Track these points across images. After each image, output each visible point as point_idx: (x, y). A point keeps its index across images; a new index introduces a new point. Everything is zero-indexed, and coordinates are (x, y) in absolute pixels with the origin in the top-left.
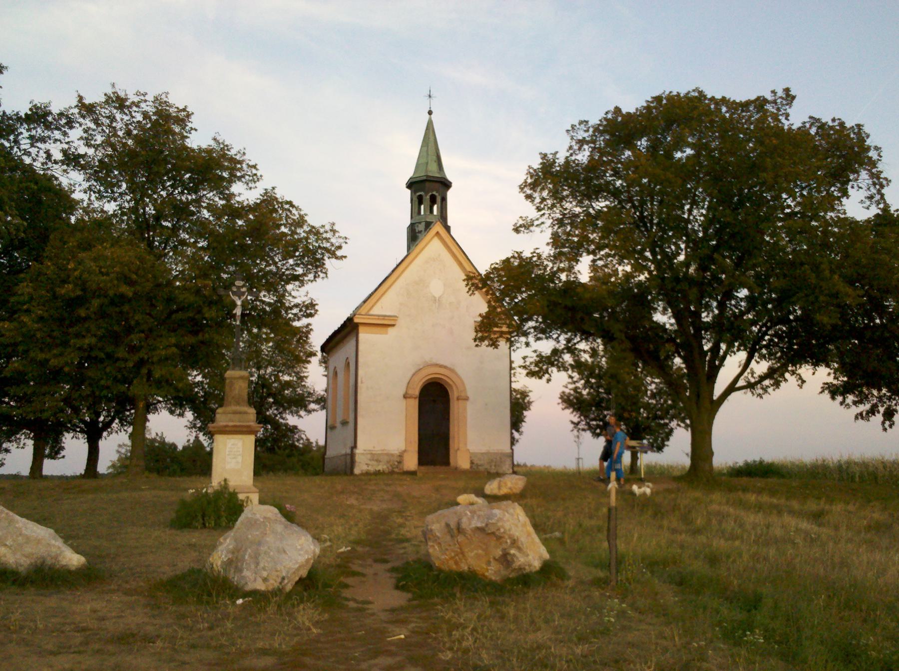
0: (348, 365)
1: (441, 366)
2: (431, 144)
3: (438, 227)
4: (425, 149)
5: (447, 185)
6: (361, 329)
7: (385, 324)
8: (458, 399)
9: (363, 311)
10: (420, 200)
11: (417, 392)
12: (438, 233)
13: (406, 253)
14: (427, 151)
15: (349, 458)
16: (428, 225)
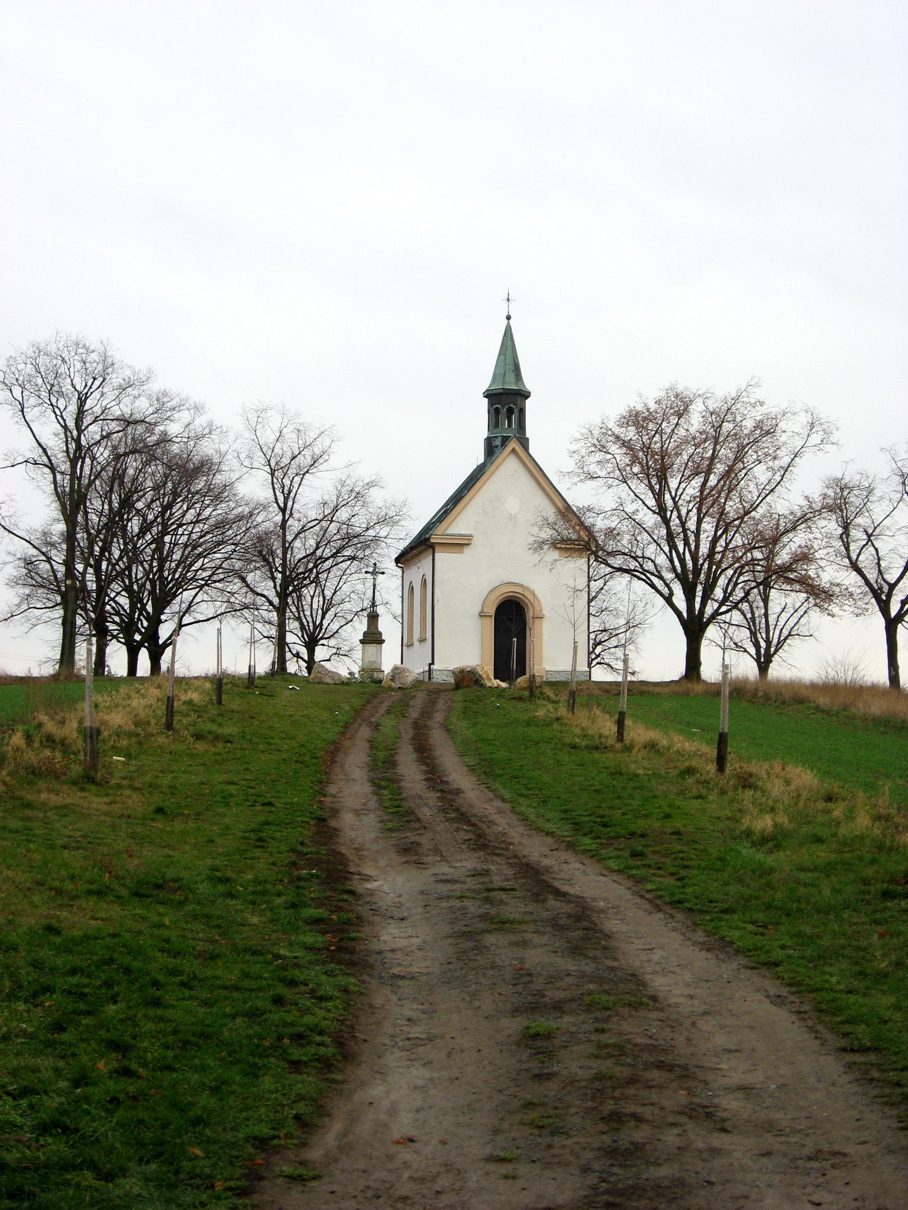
0: (424, 582)
1: (516, 584)
2: (509, 353)
3: (513, 444)
4: (502, 357)
5: (526, 395)
6: (437, 549)
7: (460, 544)
8: (534, 618)
9: (440, 530)
10: (497, 411)
11: (492, 612)
12: (514, 450)
13: (481, 460)
14: (505, 360)
15: (427, 674)
16: (505, 440)
